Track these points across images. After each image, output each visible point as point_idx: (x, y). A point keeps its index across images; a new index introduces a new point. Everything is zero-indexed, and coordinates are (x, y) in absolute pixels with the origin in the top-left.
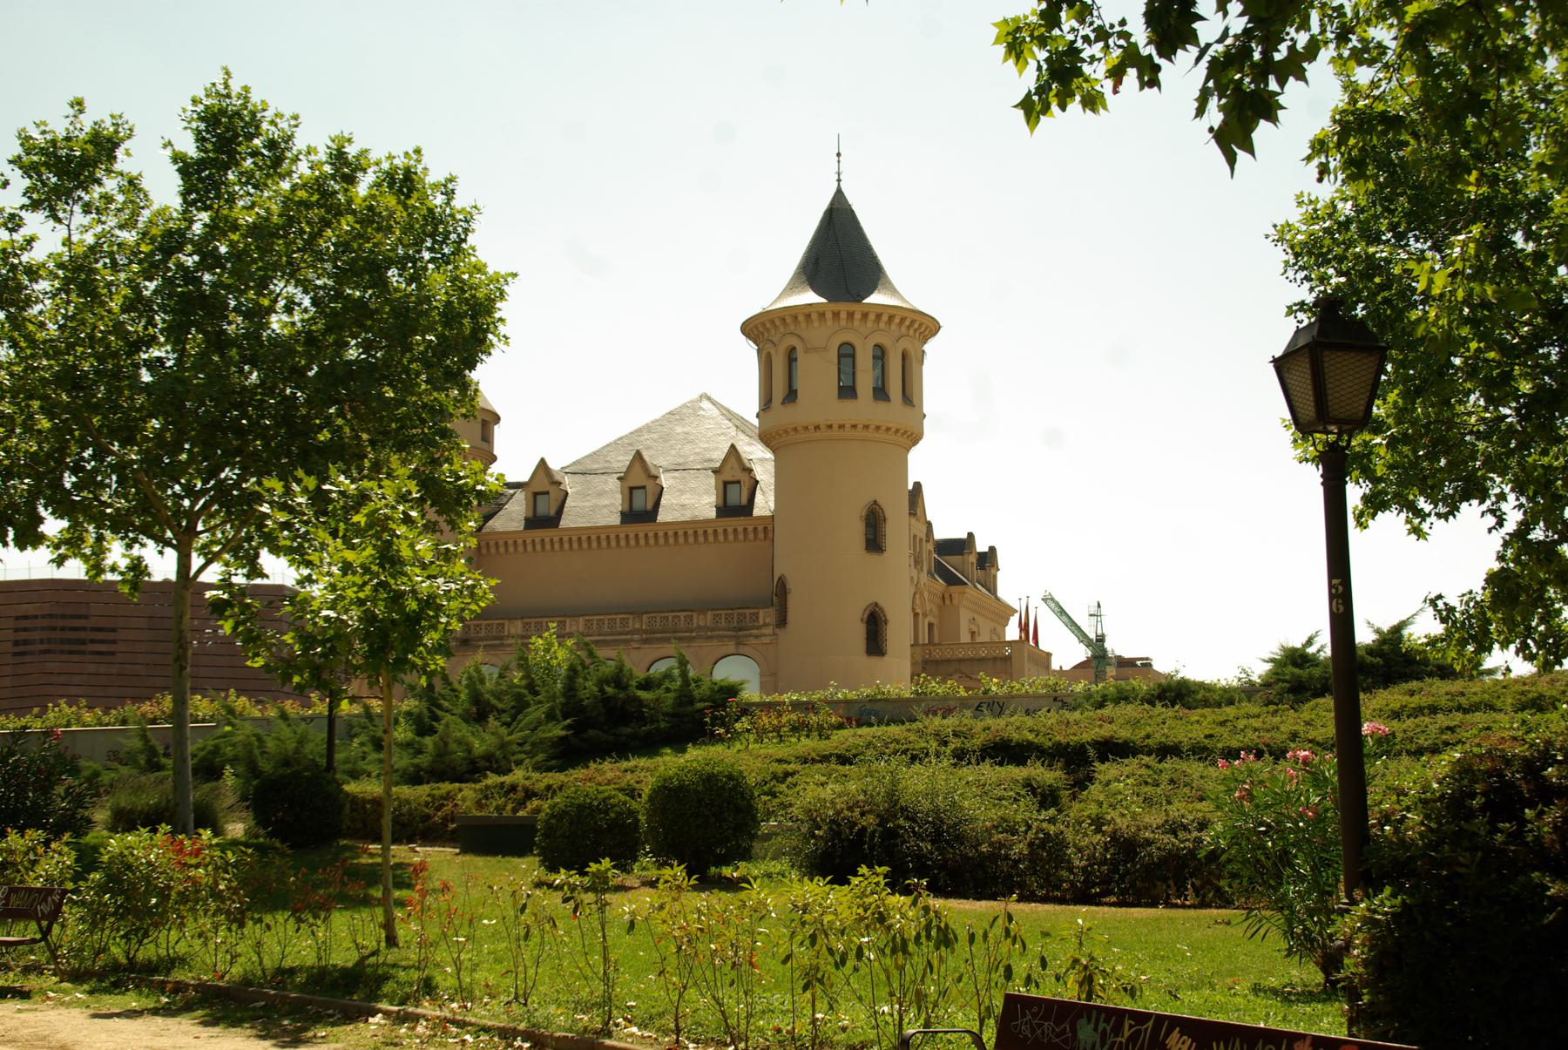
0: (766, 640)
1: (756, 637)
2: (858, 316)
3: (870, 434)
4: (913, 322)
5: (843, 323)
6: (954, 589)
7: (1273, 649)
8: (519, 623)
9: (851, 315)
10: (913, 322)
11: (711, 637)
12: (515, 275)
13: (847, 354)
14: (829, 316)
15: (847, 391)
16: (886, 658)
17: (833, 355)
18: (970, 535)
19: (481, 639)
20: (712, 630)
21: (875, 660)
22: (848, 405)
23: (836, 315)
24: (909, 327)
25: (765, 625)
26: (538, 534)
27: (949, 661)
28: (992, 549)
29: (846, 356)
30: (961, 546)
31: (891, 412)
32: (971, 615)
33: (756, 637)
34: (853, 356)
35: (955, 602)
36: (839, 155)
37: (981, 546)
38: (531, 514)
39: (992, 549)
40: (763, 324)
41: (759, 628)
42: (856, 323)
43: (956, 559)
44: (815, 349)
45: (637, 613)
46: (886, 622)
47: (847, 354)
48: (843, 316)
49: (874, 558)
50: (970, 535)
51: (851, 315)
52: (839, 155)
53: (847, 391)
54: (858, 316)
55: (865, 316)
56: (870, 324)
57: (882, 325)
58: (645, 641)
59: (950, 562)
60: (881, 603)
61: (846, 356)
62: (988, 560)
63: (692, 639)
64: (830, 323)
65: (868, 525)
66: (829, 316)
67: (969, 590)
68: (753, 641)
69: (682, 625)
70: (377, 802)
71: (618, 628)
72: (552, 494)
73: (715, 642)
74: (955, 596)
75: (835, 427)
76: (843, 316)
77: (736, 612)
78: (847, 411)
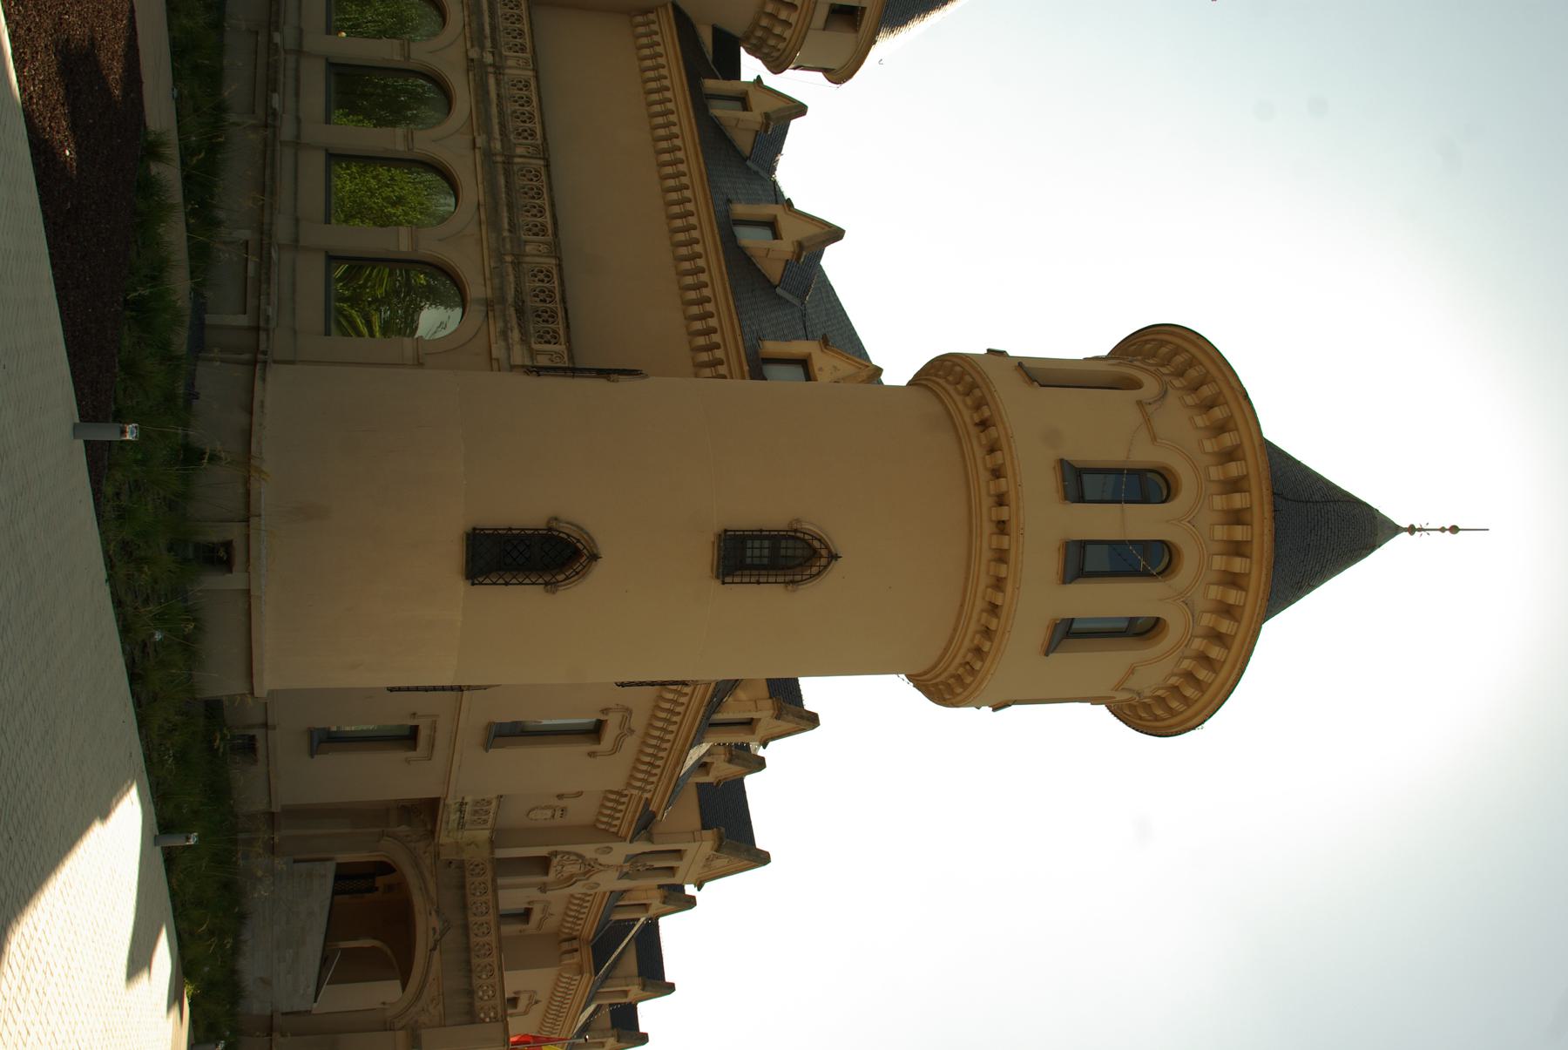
0: (498, 351)
1: (504, 334)
3: (987, 540)
6: (586, 955)
11: (500, 258)
13: (1149, 485)
16: (461, 585)
17: (1144, 455)
18: (671, 988)
20: (517, 264)
24: (1189, 676)
27: (464, 907)
28: (812, 721)
31: (1042, 595)
32: (543, 996)
36: (1454, 529)
39: (812, 721)
41: (524, 340)
43: (631, 963)
44: (1147, 420)
45: (544, 153)
46: (551, 586)
47: (1149, 485)
49: (704, 555)
50: (671, 988)
52: (1454, 529)
53: (1078, 482)
58: (488, 154)
60: (599, 571)
63: (494, 225)
65: (774, 539)
67: (586, 981)
68: (495, 328)
71: (510, 107)
74: (576, 958)
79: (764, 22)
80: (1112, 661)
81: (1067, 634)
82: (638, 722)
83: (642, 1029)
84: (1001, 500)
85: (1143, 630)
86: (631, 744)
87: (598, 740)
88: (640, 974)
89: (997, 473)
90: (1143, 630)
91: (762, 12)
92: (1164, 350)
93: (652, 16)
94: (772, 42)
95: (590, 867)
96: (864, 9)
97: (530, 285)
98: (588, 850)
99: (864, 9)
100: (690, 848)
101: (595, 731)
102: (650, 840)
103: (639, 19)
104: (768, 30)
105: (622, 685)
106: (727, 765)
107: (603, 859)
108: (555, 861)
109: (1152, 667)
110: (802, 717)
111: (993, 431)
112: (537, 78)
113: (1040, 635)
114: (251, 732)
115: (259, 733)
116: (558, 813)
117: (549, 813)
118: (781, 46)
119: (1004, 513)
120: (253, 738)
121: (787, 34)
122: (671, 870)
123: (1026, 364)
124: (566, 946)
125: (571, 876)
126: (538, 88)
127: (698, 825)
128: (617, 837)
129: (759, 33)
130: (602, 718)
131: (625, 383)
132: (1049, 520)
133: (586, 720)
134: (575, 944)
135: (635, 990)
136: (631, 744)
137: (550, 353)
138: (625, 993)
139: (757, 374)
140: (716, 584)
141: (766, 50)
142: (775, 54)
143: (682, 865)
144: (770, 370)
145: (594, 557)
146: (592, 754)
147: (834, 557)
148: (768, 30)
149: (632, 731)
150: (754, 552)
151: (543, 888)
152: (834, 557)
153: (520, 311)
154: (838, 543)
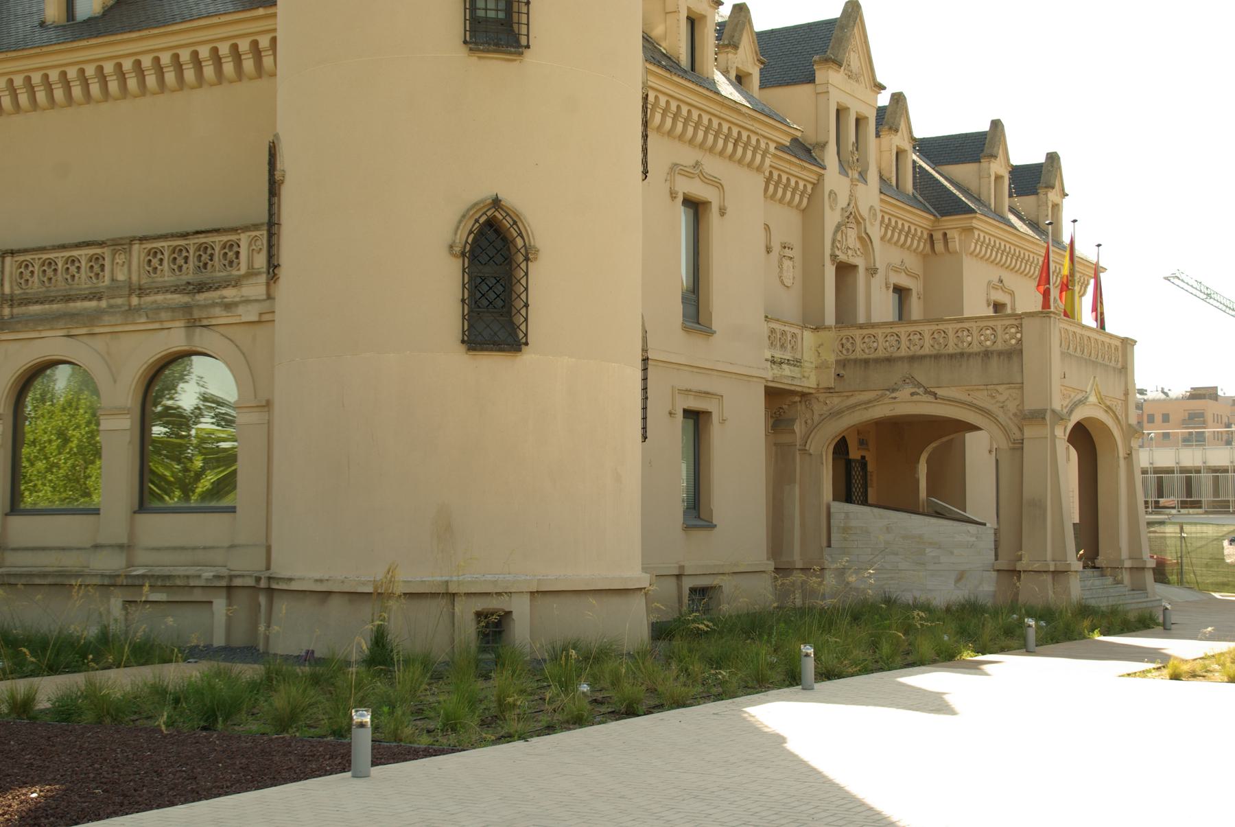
0: (249, 313)
1: (228, 306)
6: (952, 223)
11: (131, 311)
12: (1167, 278)
16: (527, 357)
20: (142, 291)
21: (491, 364)
25: (252, 273)
30: (977, 147)
33: (228, 306)
35: (955, 244)
37: (1023, 150)
49: (495, 67)
50: (996, 125)
59: (950, 177)
60: (511, 198)
62: (1036, 180)
63: (92, 318)
69: (84, 281)
70: (794, 432)
73: (142, 323)
74: (954, 235)
77: (193, 242)
86: (712, 165)
87: (706, 204)
95: (852, 217)
97: (166, 275)
98: (832, 218)
101: (695, 207)
102: (823, 146)
105: (645, 172)
107: (843, 201)
108: (842, 257)
114: (686, 592)
115: (688, 584)
116: (787, 252)
117: (787, 263)
120: (693, 590)
124: (939, 246)
125: (860, 238)
128: (818, 184)
130: (680, 199)
131: (286, 162)
133: (682, 217)
134: (938, 236)
136: (712, 165)
137: (251, 252)
138: (998, 178)
143: (855, 108)
145: (496, 202)
146: (722, 212)
151: (872, 271)
153: (201, 287)
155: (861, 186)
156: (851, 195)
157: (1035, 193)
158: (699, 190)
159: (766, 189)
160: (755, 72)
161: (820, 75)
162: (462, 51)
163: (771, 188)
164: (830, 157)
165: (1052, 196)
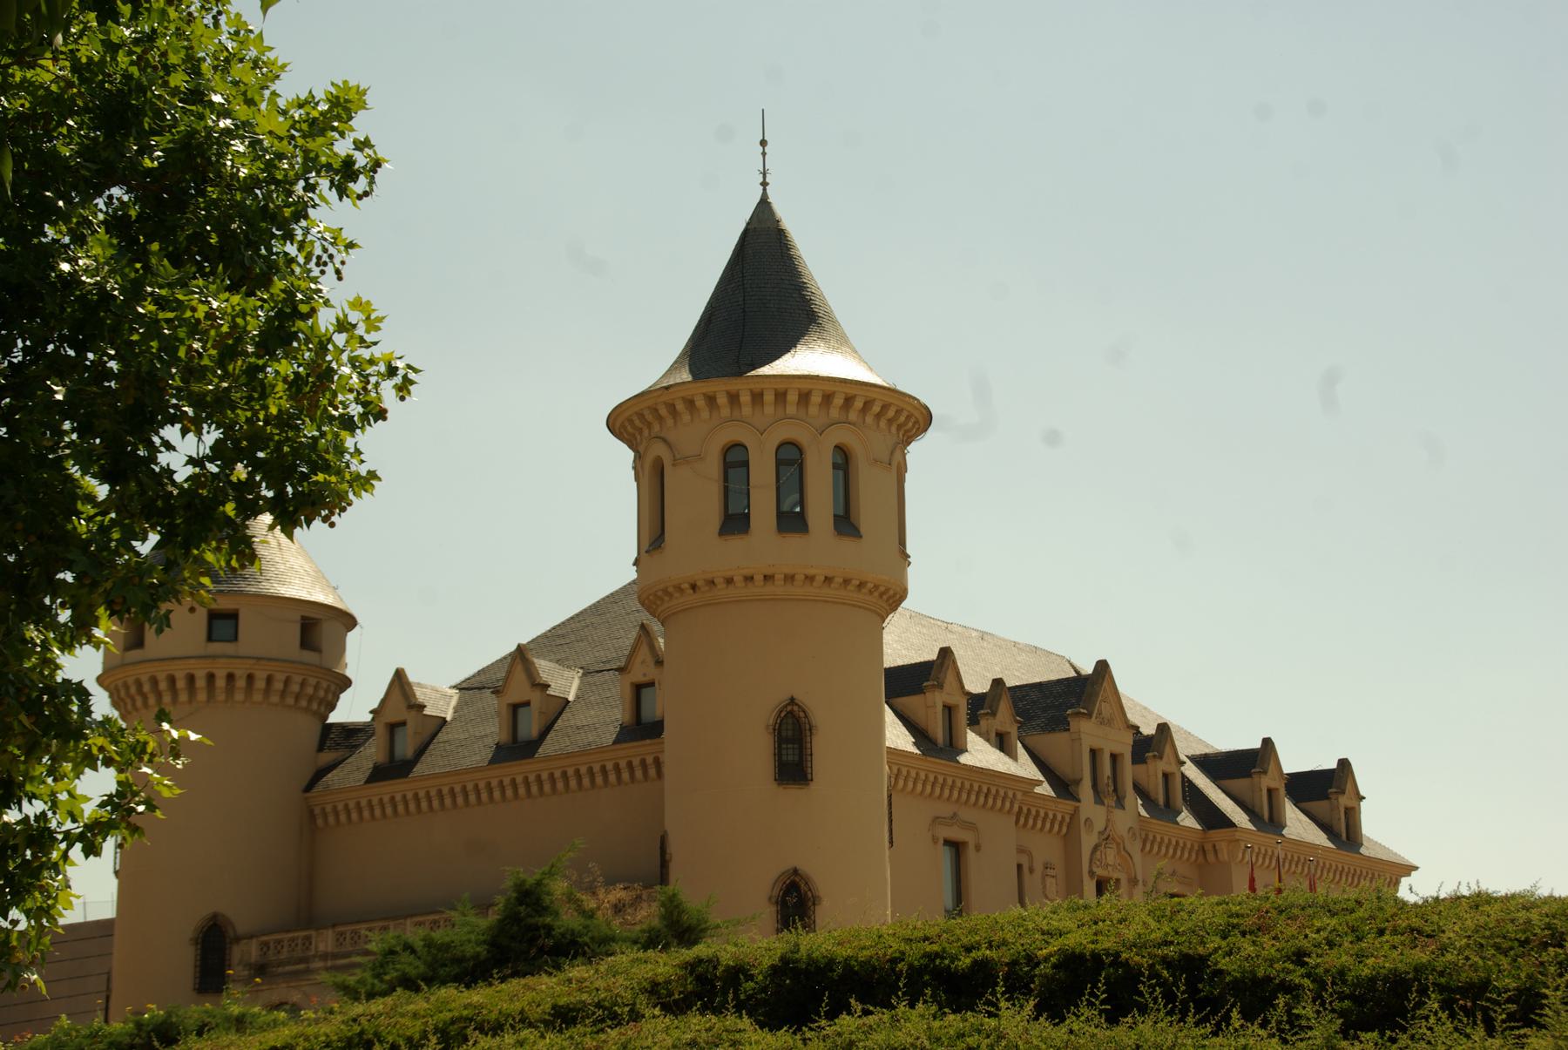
2: (745, 398)
4: (885, 407)
5: (791, 409)
6: (1217, 834)
7: (113, 876)
8: (330, 935)
9: (734, 398)
10: (885, 407)
13: (735, 461)
14: (700, 403)
15: (735, 522)
17: (714, 466)
18: (1267, 742)
19: (281, 964)
22: (736, 543)
23: (711, 400)
24: (878, 416)
26: (517, 770)
29: (790, 463)
31: (818, 547)
34: (746, 464)
35: (1224, 855)
36: (763, 143)
38: (504, 737)
40: (641, 415)
42: (747, 410)
46: (816, 900)
47: (735, 461)
48: (722, 400)
49: (793, 793)
50: (1267, 742)
51: (734, 398)
52: (763, 143)
53: (735, 522)
54: (745, 398)
55: (757, 397)
56: (769, 409)
57: (853, 416)
60: (806, 868)
61: (790, 463)
64: (705, 414)
66: (700, 403)
72: (535, 705)
74: (1223, 848)
75: (759, 578)
76: (722, 400)
78: (737, 555)
79: (304, 703)
80: (867, 480)
81: (846, 523)
82: (946, 810)
83: (1334, 765)
84: (749, 579)
85: (843, 461)
86: (967, 814)
87: (964, 844)
88: (1249, 775)
89: (729, 581)
90: (843, 461)
91: (307, 710)
92: (629, 429)
93: (317, 811)
94: (322, 693)
95: (1106, 838)
96: (303, 618)
98: (1088, 841)
99: (303, 618)
100: (1087, 743)
101: (956, 847)
102: (1078, 782)
103: (320, 822)
104: (311, 699)
105: (891, 842)
106: (999, 715)
107: (1099, 825)
108: (1100, 872)
109: (866, 443)
110: (942, 664)
111: (699, 583)
112: (412, 916)
113: (847, 544)
116: (1050, 872)
117: (1049, 881)
118: (324, 684)
119: (759, 578)
121: (313, 681)
122: (1114, 757)
123: (646, 546)
124: (1211, 857)
126: (422, 914)
127: (1066, 734)
128: (1075, 814)
129: (315, 706)
131: (673, 848)
132: (763, 543)
133: (945, 857)
134: (1208, 847)
135: (1267, 782)
136: (967, 814)
139: (654, 729)
140: (813, 785)
141: (330, 697)
142: (333, 687)
143: (1108, 748)
144: (647, 715)
145: (796, 871)
146: (978, 848)
147: (792, 701)
148: (311, 699)
149: (955, 814)
150: (790, 756)
152: (792, 701)
154: (782, 697)
155: (1118, 813)
156: (1108, 820)
157: (1327, 798)
158: (956, 834)
159: (1017, 822)
160: (1013, 730)
161: (1074, 724)
162: (774, 785)
163: (1022, 820)
164: (1086, 791)
165: (1344, 801)
